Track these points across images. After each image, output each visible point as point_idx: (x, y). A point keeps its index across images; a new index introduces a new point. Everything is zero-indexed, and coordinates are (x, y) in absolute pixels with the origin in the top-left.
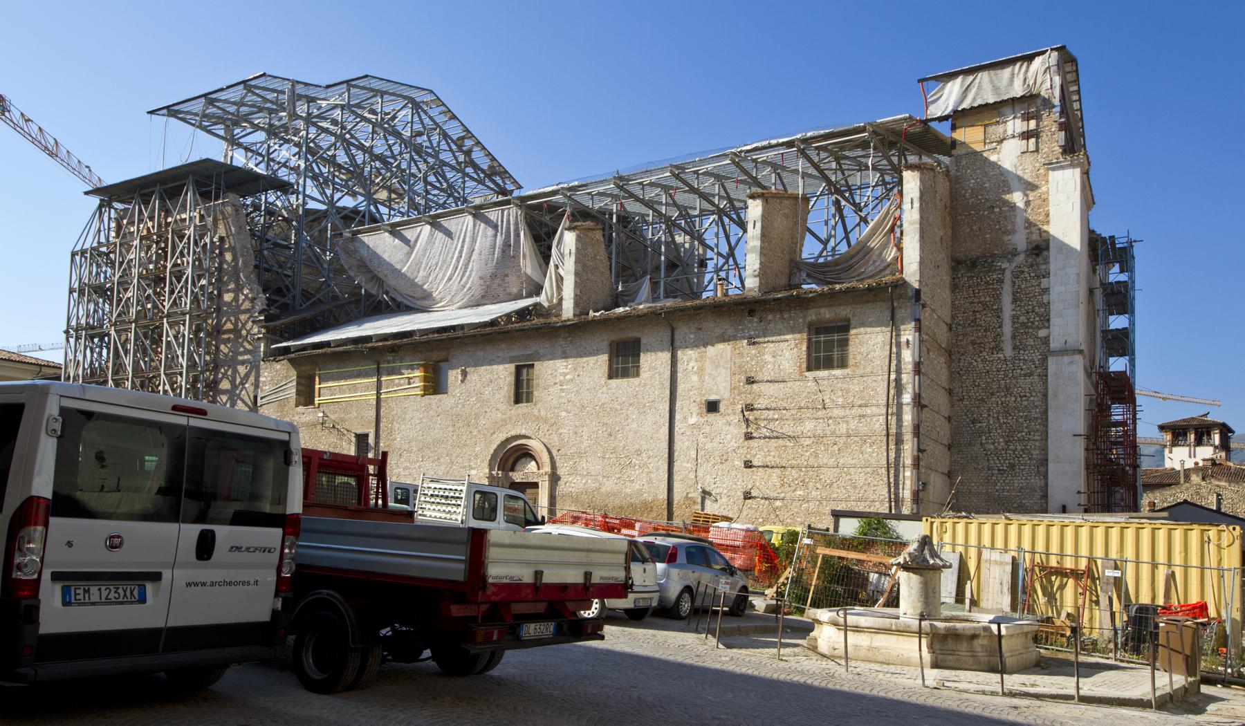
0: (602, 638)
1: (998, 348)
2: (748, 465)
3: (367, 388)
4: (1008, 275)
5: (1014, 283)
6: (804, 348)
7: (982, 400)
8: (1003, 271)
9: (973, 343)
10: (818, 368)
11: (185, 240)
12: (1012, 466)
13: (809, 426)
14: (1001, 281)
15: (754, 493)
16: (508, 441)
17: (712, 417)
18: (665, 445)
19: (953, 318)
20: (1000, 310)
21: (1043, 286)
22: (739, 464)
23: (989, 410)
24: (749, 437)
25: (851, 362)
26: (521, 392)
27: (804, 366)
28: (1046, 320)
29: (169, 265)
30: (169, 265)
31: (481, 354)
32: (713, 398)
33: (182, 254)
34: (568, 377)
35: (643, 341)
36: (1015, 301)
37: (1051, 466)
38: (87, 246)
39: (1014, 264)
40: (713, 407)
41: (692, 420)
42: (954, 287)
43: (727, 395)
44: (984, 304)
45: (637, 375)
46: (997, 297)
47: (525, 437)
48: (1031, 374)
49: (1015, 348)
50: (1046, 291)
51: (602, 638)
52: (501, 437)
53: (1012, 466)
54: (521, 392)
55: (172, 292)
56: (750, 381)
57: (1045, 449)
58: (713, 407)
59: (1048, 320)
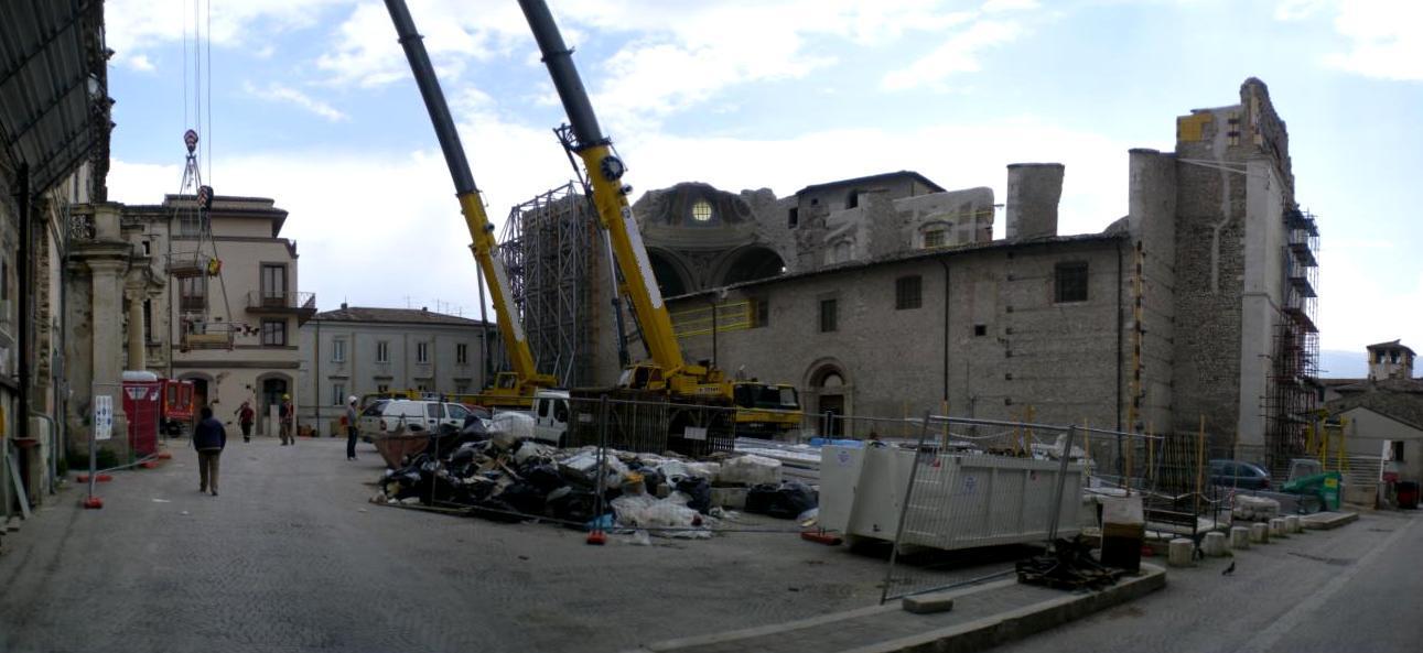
0: (629, 189)
1: (1208, 287)
2: (1008, 377)
3: (706, 326)
4: (1216, 233)
5: (1220, 239)
6: (1052, 283)
7: (1197, 326)
8: (1212, 229)
9: (1190, 282)
10: (1063, 300)
11: (569, 228)
12: (1216, 378)
13: (1056, 347)
14: (1211, 237)
15: (1013, 400)
16: (818, 361)
17: (981, 339)
18: (943, 362)
19: (1176, 262)
20: (1210, 259)
21: (1241, 243)
22: (1001, 376)
23: (1201, 334)
24: (1009, 355)
25: (1089, 295)
26: (828, 320)
27: (1053, 299)
28: (1242, 268)
29: (560, 245)
30: (560, 245)
31: (793, 293)
32: (981, 323)
33: (567, 237)
34: (864, 309)
35: (924, 278)
36: (1221, 252)
37: (1243, 378)
38: (506, 240)
39: (1222, 225)
40: (980, 331)
41: (965, 341)
42: (1177, 240)
43: (992, 320)
44: (1199, 253)
45: (1180, 121)
46: (1209, 249)
47: (833, 358)
48: (1231, 308)
49: (1220, 287)
50: (1243, 247)
51: (629, 189)
52: (811, 360)
53: (1216, 378)
54: (828, 320)
55: (563, 264)
56: (1010, 310)
57: (1238, 366)
58: (980, 331)
59: (1243, 269)
